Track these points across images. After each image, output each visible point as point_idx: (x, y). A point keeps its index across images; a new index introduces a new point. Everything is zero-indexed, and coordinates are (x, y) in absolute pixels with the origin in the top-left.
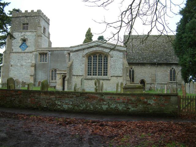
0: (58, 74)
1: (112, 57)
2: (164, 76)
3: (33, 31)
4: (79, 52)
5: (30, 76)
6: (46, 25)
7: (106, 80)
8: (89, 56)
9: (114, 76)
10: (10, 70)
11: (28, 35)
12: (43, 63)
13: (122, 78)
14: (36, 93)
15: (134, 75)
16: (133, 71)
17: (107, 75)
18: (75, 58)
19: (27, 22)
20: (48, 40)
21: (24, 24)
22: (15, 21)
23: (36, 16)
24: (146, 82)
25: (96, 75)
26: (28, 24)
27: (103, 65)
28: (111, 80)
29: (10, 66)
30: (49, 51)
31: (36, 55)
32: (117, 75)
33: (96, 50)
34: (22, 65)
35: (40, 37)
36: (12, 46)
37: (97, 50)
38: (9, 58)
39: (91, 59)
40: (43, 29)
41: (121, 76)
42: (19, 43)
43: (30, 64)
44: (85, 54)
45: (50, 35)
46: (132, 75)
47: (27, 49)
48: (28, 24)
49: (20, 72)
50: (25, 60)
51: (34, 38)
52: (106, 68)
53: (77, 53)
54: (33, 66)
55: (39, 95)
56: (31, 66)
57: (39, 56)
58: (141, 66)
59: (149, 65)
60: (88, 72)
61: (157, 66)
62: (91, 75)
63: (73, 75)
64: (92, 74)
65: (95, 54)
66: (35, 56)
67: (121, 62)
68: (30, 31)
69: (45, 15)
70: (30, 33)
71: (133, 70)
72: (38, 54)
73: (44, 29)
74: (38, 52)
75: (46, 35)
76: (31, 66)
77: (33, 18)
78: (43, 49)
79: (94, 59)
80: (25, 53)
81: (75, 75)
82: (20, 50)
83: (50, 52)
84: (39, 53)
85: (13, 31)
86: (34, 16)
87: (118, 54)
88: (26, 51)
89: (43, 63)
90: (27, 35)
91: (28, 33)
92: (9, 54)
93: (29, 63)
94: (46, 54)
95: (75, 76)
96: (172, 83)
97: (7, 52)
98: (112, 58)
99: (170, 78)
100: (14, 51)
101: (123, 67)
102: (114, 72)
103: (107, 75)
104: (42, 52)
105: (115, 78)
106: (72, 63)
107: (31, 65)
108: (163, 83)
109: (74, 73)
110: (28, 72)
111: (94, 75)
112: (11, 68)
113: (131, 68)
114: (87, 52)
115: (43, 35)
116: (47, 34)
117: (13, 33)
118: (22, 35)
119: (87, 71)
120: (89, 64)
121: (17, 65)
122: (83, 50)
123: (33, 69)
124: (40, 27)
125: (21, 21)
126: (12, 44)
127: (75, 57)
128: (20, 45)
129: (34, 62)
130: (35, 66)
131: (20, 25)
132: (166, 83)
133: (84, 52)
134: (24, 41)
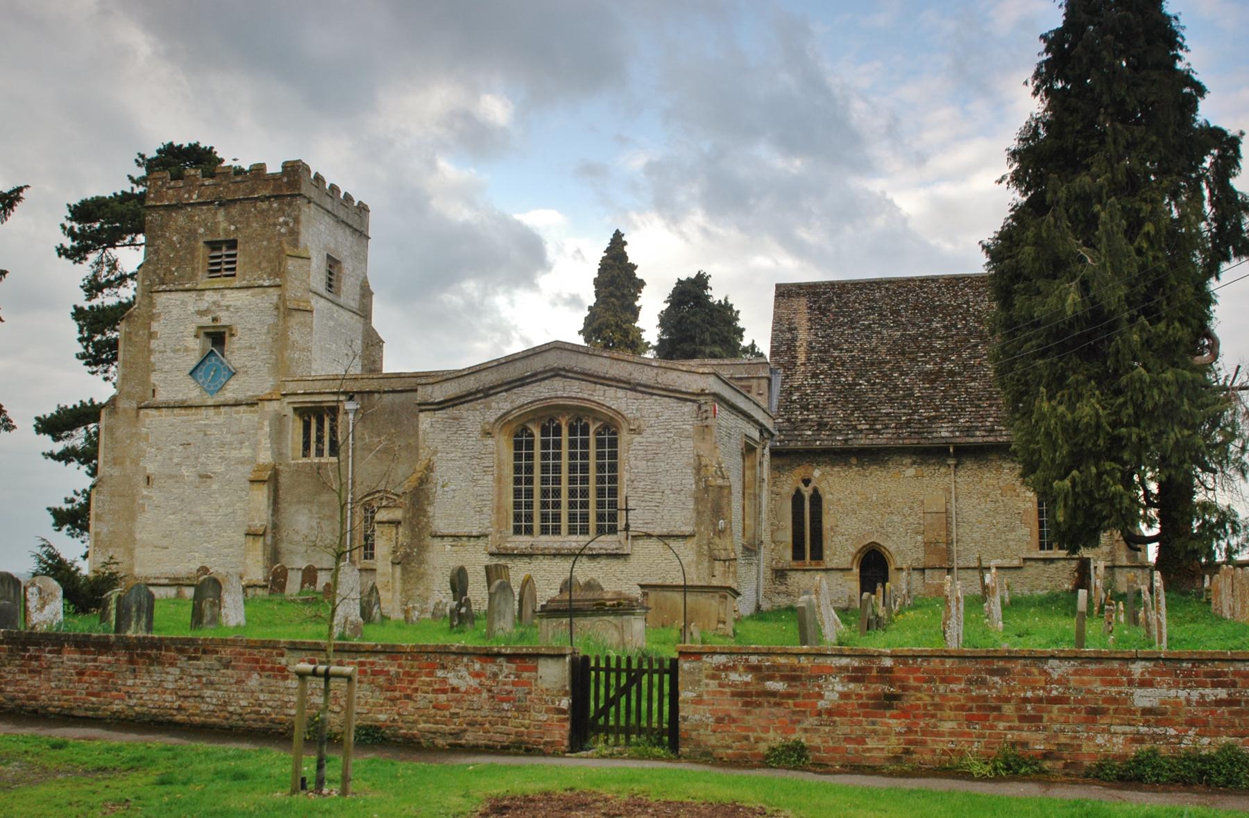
0: (386, 528)
1: (637, 431)
2: (1001, 519)
3: (261, 282)
4: (463, 410)
5: (242, 539)
6: (343, 243)
10: (143, 505)
11: (237, 309)
13: (691, 543)
14: (46, 646)
15: (820, 522)
16: (816, 499)
18: (443, 441)
19: (226, 231)
21: (213, 245)
22: (162, 228)
24: (896, 561)
25: (557, 530)
26: (233, 244)
27: (565, 475)
28: (632, 559)
29: (143, 483)
30: (351, 396)
31: (280, 419)
32: (665, 531)
33: (553, 394)
34: (205, 477)
35: (298, 318)
36: (149, 368)
37: (559, 393)
39: (530, 445)
40: (324, 265)
41: (684, 537)
42: (186, 350)
43: (247, 471)
44: (497, 420)
47: (233, 384)
48: (233, 244)
49: (191, 518)
50: (223, 445)
51: (270, 320)
52: (609, 490)
53: (453, 412)
54: (264, 482)
55: (59, 652)
56: (252, 481)
57: (294, 428)
58: (861, 464)
59: (907, 461)
60: (517, 517)
61: (956, 466)
62: (529, 531)
63: (435, 536)
64: (537, 523)
65: (548, 416)
66: (271, 425)
67: (685, 460)
68: (244, 283)
69: (334, 188)
70: (250, 292)
71: (815, 490)
72: (289, 411)
73: (333, 264)
75: (342, 300)
76: (252, 481)
77: (262, 212)
78: (318, 386)
79: (545, 445)
80: (222, 409)
81: (446, 532)
82: (191, 391)
83: (351, 399)
84: (295, 409)
85: (151, 285)
86: (268, 198)
87: (667, 414)
88: (229, 395)
89: (316, 460)
90: (228, 307)
91: (236, 294)
92: (134, 413)
93: (242, 462)
94: (334, 411)
95: (442, 537)
96: (1052, 560)
97: (123, 404)
98: (638, 438)
99: (1036, 528)
100: (162, 396)
101: (696, 483)
104: (308, 399)
105: (654, 546)
106: (429, 468)
107: (252, 477)
109: (440, 525)
110: (240, 512)
111: (544, 531)
112: (145, 493)
113: (807, 482)
114: (507, 406)
115: (318, 304)
117: (155, 295)
118: (203, 305)
119: (511, 511)
120: (522, 473)
121: (177, 478)
122: (486, 396)
123: (261, 496)
124: (305, 261)
125: (196, 231)
126: (152, 359)
128: (195, 363)
129: (266, 457)
130: (272, 480)
131: (192, 251)
132: (1016, 563)
133: (490, 408)
134: (217, 337)
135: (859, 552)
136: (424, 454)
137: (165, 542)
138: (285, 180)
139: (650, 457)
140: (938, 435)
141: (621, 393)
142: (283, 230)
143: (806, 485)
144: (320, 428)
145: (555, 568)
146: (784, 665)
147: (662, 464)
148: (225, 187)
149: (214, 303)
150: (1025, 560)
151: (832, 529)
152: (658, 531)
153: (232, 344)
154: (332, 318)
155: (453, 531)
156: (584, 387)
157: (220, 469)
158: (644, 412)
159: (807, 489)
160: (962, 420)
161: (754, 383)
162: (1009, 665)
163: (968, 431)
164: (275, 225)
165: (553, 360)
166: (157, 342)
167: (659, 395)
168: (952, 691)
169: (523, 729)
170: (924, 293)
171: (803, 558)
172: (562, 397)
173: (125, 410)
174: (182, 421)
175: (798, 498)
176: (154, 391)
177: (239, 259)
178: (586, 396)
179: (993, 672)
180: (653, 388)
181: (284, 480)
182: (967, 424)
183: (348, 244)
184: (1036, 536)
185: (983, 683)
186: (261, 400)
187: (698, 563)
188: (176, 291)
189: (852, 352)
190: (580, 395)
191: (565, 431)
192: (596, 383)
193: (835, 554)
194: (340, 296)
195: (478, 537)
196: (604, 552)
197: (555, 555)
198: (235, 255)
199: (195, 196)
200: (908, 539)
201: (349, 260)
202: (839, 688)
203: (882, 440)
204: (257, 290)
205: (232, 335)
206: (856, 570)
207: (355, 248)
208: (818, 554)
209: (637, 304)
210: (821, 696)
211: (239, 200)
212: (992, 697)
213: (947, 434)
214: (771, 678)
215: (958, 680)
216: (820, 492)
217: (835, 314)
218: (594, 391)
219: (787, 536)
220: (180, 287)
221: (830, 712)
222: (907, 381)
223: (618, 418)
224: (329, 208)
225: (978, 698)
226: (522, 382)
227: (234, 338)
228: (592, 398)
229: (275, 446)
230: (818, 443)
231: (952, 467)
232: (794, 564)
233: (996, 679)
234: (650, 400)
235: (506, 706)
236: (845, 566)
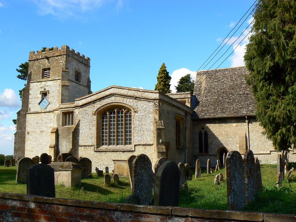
6: (82, 68)
7: (128, 151)
11: (50, 86)
12: (68, 126)
17: (130, 143)
21: (44, 70)
22: (32, 66)
23: (60, 55)
26: (49, 69)
32: (144, 143)
33: (112, 102)
37: (114, 101)
38: (25, 121)
42: (38, 98)
43: (50, 130)
45: (91, 83)
46: (205, 141)
50: (46, 123)
53: (84, 108)
54: (54, 132)
56: (51, 133)
67: (150, 120)
68: (52, 79)
74: (61, 110)
80: (46, 113)
82: (38, 109)
89: (68, 126)
90: (48, 86)
94: (72, 113)
97: (22, 113)
98: (136, 114)
100: (32, 110)
102: (139, 138)
103: (130, 143)
106: (78, 125)
108: (261, 152)
112: (28, 136)
113: (203, 129)
114: (99, 106)
116: (83, 80)
118: (42, 86)
123: (54, 136)
127: (82, 116)
129: (56, 126)
132: (269, 152)
134: (45, 94)
135: (219, 150)
136: (76, 122)
137: (32, 150)
138: (62, 51)
139: (140, 120)
140: (242, 113)
141: (131, 100)
142: (61, 64)
143: (203, 130)
145: (113, 155)
147: (144, 122)
148: (48, 54)
149: (44, 85)
150: (271, 151)
151: (211, 143)
152: (143, 143)
153: (49, 96)
154: (77, 88)
155: (84, 144)
156: (121, 99)
157: (45, 129)
158: (138, 106)
159: (203, 131)
160: (250, 108)
161: (187, 99)
164: (60, 63)
166: (31, 96)
167: (143, 100)
170: (240, 71)
171: (202, 152)
172: (115, 102)
173: (22, 114)
174: (36, 117)
175: (200, 134)
176: (30, 109)
178: (121, 102)
180: (141, 98)
181: (60, 132)
182: (251, 109)
183: (83, 68)
186: (54, 110)
188: (35, 82)
189: (218, 89)
190: (119, 102)
192: (124, 98)
193: (212, 151)
194: (80, 82)
195: (91, 146)
196: (126, 150)
197: (112, 151)
198: (50, 72)
199: (40, 57)
200: (234, 145)
201: (83, 73)
203: (225, 115)
204: (55, 81)
205: (49, 93)
207: (86, 70)
208: (207, 151)
209: (170, 83)
211: (51, 57)
213: (245, 113)
216: (207, 132)
217: (214, 79)
218: (124, 100)
219: (197, 145)
220: (36, 81)
222: (234, 97)
223: (131, 108)
224: (76, 58)
227: (49, 94)
228: (123, 102)
229: (58, 123)
230: (206, 117)
231: (247, 123)
234: (140, 102)
236: (215, 154)
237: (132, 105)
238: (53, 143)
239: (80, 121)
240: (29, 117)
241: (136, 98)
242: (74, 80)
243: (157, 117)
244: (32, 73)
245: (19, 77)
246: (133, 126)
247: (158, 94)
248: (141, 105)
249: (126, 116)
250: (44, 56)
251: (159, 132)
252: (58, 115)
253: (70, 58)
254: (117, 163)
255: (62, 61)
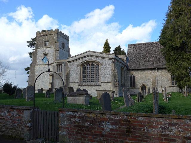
1: (102, 65)
4: (74, 63)
6: (65, 41)
8: (82, 65)
9: (104, 82)
17: (98, 82)
20: (68, 53)
21: (45, 41)
25: (89, 82)
26: (48, 41)
38: (35, 69)
52: (98, 76)
53: (73, 63)
62: (85, 82)
65: (87, 62)
74: (55, 63)
82: (42, 63)
97: (33, 65)
98: (102, 66)
100: (38, 63)
103: (98, 82)
105: (105, 84)
106: (69, 72)
116: (66, 48)
118: (44, 50)
132: (168, 87)
134: (46, 55)
141: (99, 59)
144: (60, 68)
146: (91, 117)
153: (48, 56)
162: (179, 122)
163: (159, 66)
165: (88, 53)
168: (154, 131)
169: (19, 132)
175: (131, 77)
177: (49, 43)
179: (171, 125)
184: (171, 83)
185: (167, 129)
187: (112, 87)
191: (91, 65)
202: (110, 127)
206: (141, 88)
210: (103, 129)
212: (171, 135)
214: (87, 121)
215: (157, 127)
221: (106, 136)
225: (165, 135)
226: (84, 57)
232: (131, 87)
233: (173, 128)
235: (15, 124)
237: (100, 61)
238: (51, 81)
239: (70, 69)
240: (37, 67)
241: (102, 57)
242: (61, 47)
243: (113, 67)
244: (38, 43)
245: (28, 46)
246: (100, 72)
247: (114, 56)
248: (104, 61)
249: (96, 67)
250: (45, 34)
251: (114, 76)
252: (54, 66)
253: (59, 36)
254: (99, 92)
255: (55, 37)
